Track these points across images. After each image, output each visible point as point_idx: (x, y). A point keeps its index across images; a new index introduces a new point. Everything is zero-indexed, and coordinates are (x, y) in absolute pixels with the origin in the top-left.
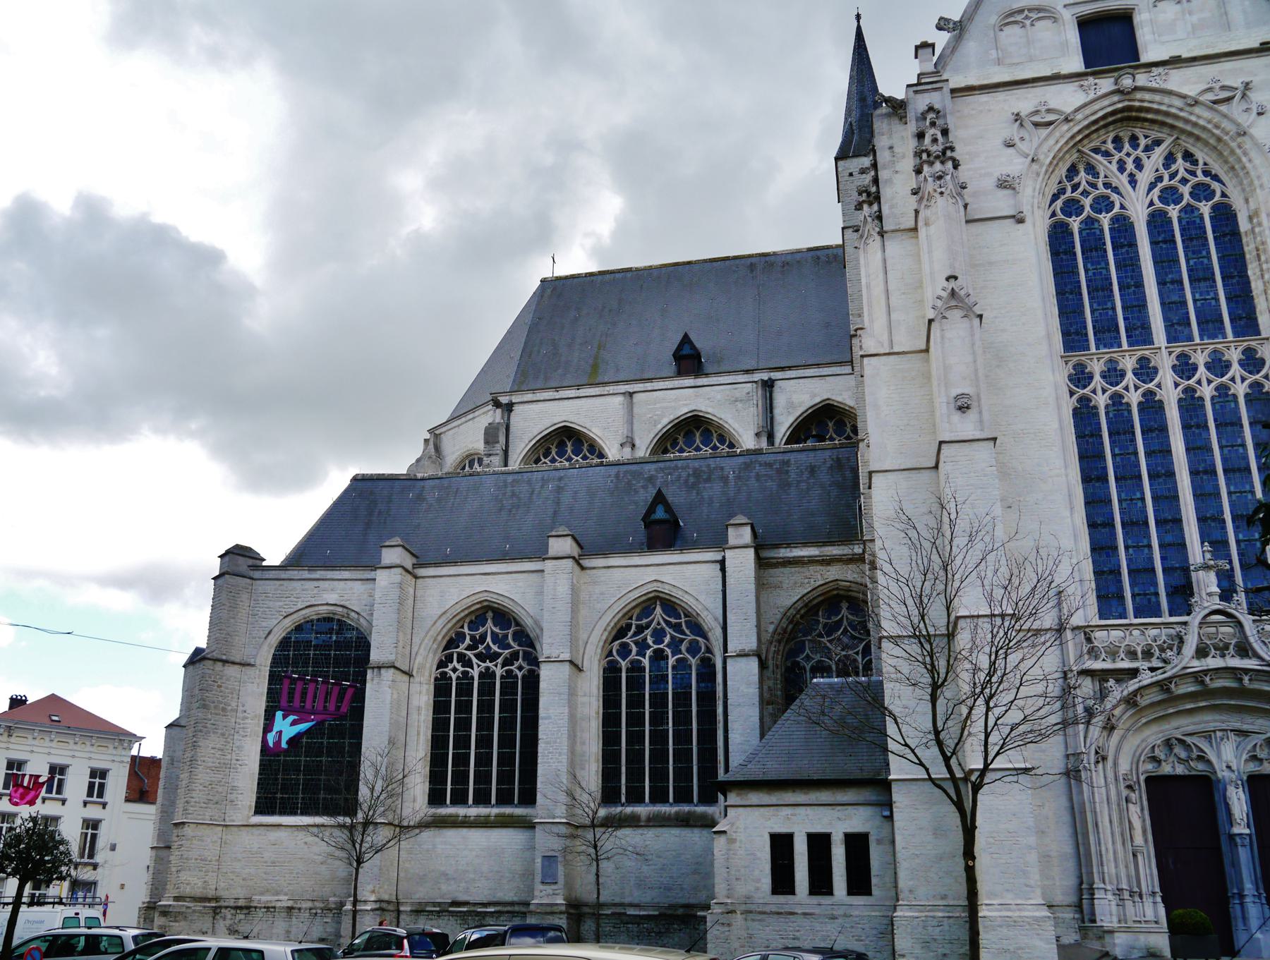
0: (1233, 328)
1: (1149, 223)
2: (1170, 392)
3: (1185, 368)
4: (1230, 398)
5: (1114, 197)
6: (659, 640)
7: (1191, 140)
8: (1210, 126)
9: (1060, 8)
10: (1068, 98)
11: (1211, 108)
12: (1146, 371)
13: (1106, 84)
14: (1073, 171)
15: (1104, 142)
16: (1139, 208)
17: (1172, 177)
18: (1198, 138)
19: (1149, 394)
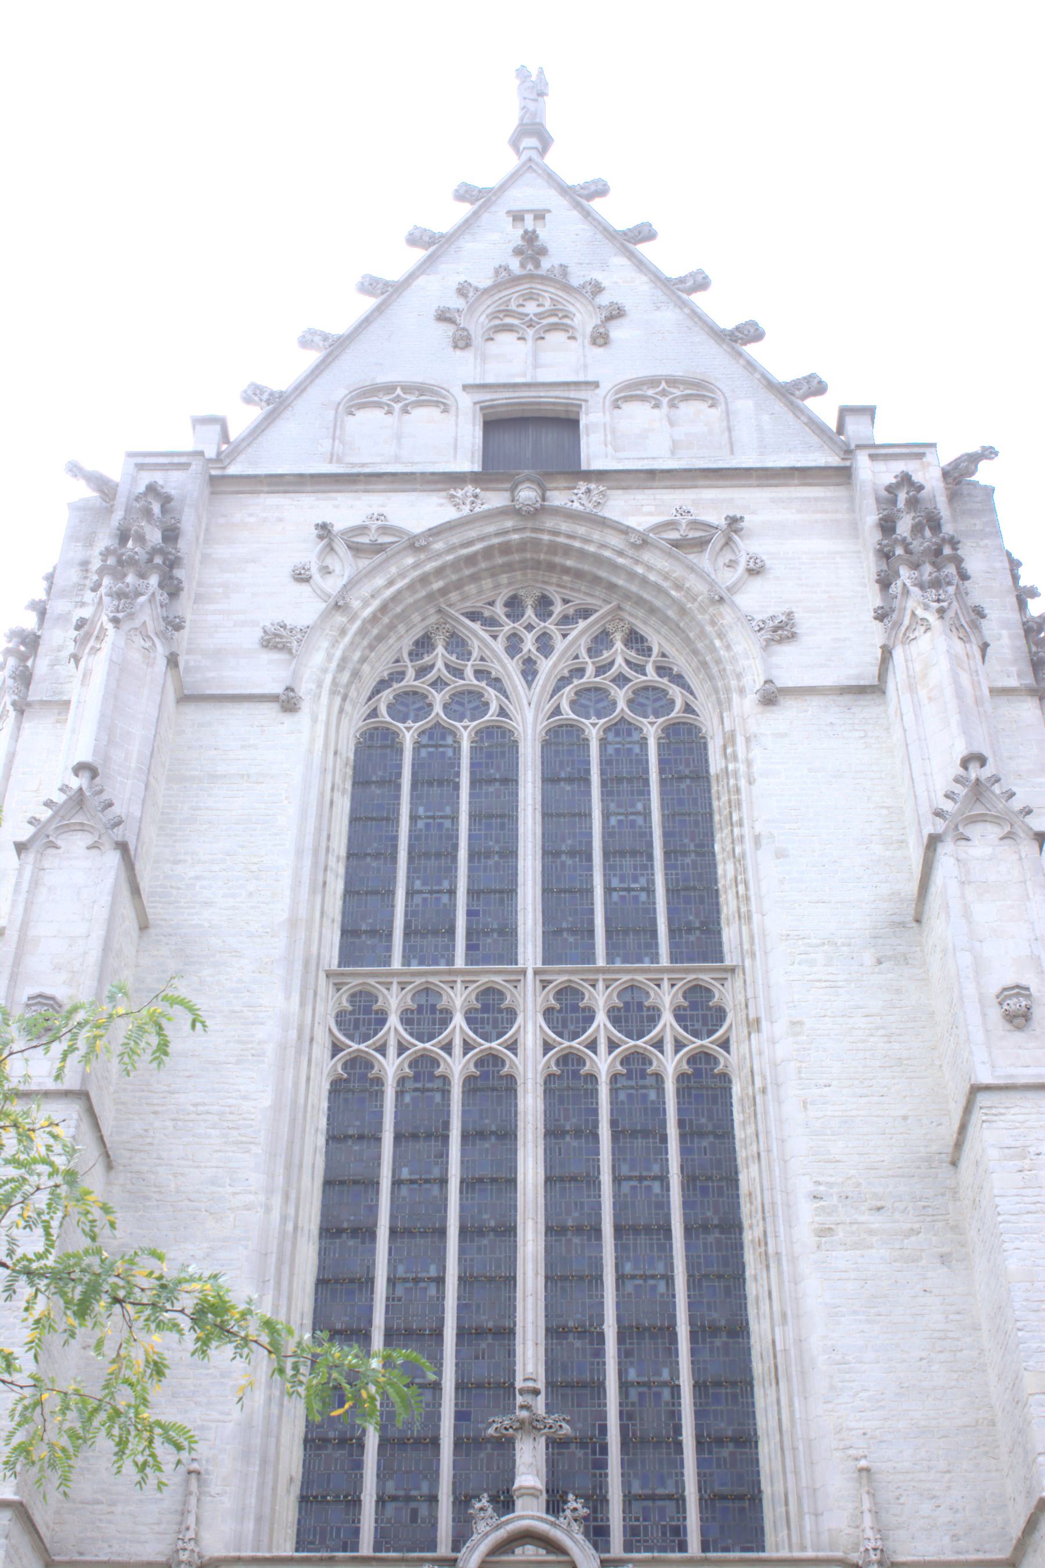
0: (673, 945)
1: (546, 745)
3: (568, 1014)
4: (650, 1081)
5: (491, 694)
7: (641, 613)
8: (666, 585)
9: (457, 391)
10: (420, 513)
11: (670, 555)
12: (492, 1013)
13: (495, 500)
14: (423, 644)
15: (492, 604)
16: (530, 715)
17: (601, 670)
18: (652, 610)
19: (490, 1062)
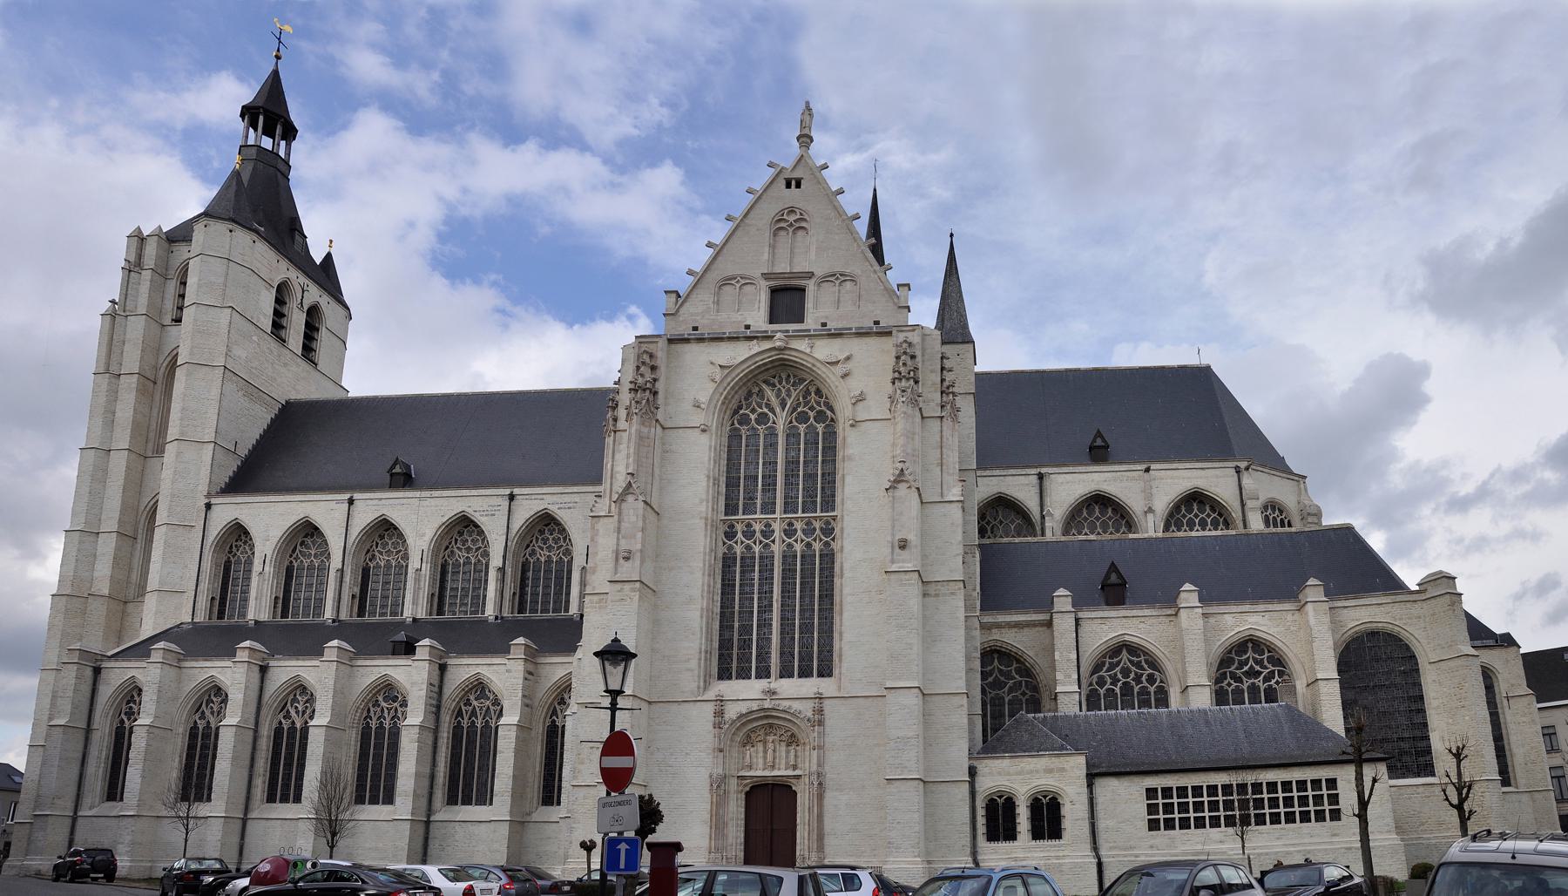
2: (777, 549)
6: (1126, 675)
